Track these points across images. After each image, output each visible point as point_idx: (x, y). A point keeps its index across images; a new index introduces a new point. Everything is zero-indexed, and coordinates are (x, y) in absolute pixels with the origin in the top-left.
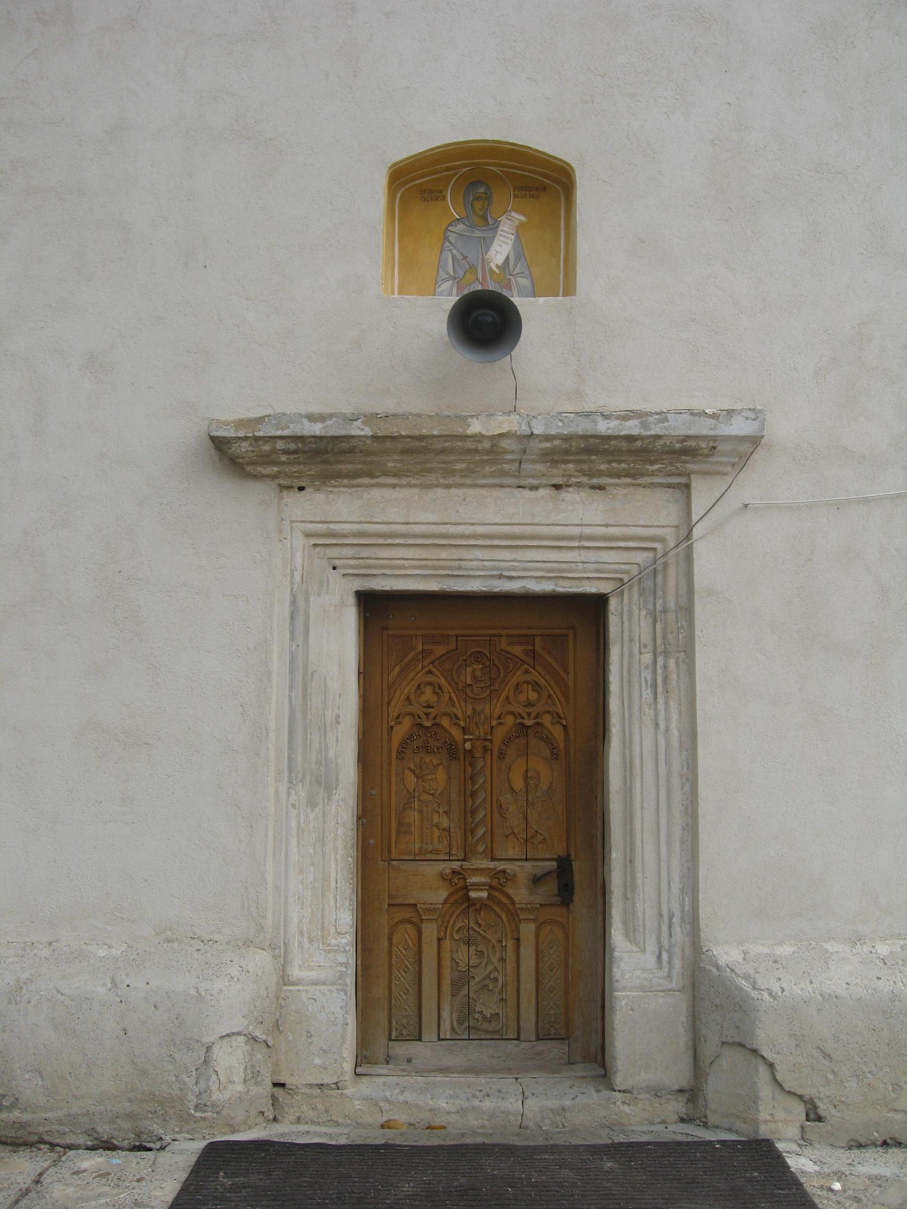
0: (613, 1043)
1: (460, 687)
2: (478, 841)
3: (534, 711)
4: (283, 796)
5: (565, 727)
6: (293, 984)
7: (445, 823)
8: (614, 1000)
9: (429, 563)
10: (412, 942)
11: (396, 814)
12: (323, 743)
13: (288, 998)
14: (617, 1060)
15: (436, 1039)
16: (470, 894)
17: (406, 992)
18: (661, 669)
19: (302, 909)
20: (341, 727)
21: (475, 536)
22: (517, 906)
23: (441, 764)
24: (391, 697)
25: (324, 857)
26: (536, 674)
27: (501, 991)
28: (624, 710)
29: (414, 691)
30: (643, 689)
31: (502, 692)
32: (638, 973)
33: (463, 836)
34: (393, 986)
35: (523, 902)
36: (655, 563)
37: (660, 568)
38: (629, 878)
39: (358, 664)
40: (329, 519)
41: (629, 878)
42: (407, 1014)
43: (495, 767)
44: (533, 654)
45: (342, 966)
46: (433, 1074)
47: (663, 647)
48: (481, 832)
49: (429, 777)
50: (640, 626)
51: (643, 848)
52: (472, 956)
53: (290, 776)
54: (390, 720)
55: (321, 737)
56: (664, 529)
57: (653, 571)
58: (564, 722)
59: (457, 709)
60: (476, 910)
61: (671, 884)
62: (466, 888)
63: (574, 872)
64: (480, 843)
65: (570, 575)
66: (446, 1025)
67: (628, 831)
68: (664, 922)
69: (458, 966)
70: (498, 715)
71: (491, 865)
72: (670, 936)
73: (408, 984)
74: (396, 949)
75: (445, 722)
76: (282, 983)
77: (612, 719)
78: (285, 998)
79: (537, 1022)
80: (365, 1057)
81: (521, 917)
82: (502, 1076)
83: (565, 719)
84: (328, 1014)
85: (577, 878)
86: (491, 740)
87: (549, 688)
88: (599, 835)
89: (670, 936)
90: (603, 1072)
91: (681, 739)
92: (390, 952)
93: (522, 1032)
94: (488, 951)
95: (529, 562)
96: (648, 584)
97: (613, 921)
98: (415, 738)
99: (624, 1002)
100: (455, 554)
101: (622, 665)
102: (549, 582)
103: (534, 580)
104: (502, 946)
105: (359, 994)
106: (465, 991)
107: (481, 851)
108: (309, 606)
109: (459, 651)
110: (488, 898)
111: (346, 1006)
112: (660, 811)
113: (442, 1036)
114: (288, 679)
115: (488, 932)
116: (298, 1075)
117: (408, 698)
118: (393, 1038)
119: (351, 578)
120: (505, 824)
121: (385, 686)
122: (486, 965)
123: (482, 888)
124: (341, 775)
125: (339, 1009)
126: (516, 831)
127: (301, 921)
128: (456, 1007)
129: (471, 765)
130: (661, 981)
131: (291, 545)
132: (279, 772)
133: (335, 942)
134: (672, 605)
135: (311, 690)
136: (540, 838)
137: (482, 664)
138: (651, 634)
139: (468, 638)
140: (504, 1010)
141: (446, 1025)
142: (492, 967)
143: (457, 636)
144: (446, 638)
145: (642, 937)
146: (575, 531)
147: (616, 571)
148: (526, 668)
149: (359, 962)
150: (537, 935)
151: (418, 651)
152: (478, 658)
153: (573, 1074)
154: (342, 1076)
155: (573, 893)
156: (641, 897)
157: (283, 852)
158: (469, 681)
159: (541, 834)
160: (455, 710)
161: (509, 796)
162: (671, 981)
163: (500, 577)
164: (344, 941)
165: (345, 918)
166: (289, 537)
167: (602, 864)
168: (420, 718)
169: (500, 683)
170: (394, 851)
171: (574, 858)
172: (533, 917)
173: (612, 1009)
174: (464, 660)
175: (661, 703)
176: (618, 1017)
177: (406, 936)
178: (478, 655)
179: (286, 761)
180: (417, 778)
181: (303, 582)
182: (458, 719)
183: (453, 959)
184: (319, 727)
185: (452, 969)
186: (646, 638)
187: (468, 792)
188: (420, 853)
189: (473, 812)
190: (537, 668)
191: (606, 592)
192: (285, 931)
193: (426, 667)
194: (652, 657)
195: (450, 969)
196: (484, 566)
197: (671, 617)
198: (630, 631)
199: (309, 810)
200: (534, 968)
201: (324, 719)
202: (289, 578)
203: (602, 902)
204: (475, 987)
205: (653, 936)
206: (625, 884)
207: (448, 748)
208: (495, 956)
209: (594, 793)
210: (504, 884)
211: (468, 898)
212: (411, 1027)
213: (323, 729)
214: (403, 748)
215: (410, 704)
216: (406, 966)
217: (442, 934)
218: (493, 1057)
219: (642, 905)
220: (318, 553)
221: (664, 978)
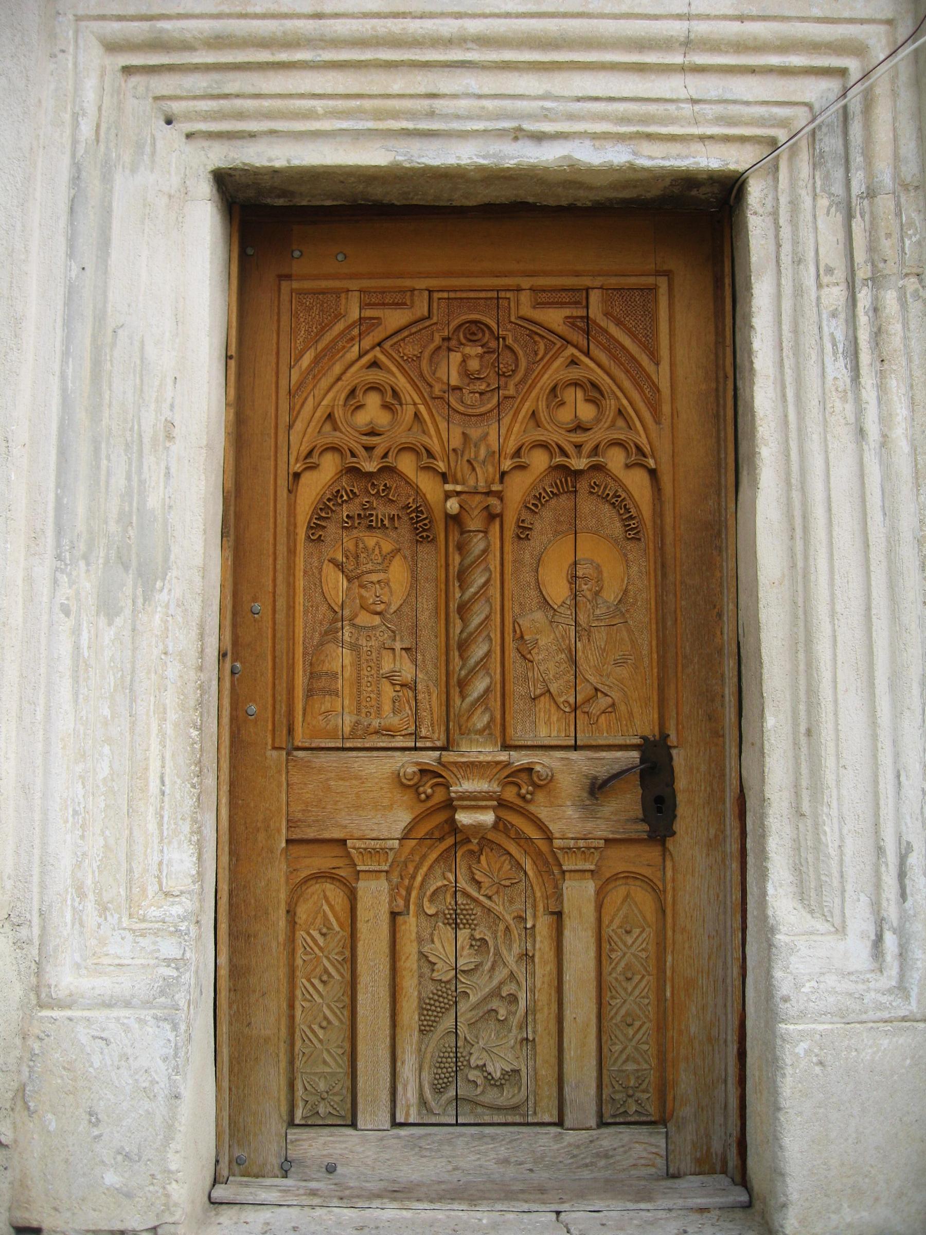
0: (776, 1139)
1: (437, 391)
2: (474, 704)
3: (589, 440)
4: (43, 588)
5: (653, 473)
6: (61, 1005)
7: (407, 671)
8: (779, 1042)
9: (367, 104)
10: (337, 920)
11: (305, 654)
12: (135, 478)
13: (48, 1036)
14: (788, 1180)
15: (387, 1125)
16: (457, 817)
17: (324, 1024)
18: (866, 313)
19: (82, 837)
20: (175, 448)
21: (461, 41)
22: (557, 843)
23: (399, 550)
24: (295, 413)
25: (133, 724)
26: (592, 365)
27: (524, 1025)
28: (785, 407)
29: (341, 402)
30: (829, 359)
31: (523, 401)
32: (831, 981)
33: (444, 697)
34: (298, 1012)
35: (571, 835)
36: (844, 95)
37: (855, 106)
38: (804, 770)
39: (224, 335)
40: (155, 10)
41: (804, 770)
42: (329, 1070)
43: (509, 558)
44: (586, 326)
45: (169, 966)
46: (376, 1203)
47: (869, 267)
48: (479, 686)
49: (374, 577)
50: (816, 229)
51: (836, 701)
52: (463, 948)
53: (58, 545)
54: (292, 461)
55: (130, 464)
56: (865, 27)
57: (841, 111)
58: (651, 463)
59: (430, 437)
60: (471, 852)
61: (903, 778)
62: (449, 806)
63: (676, 769)
64: (479, 711)
65: (664, 130)
66: (409, 1094)
67: (802, 667)
68: (887, 865)
69: (433, 970)
70: (516, 447)
71: (503, 757)
72: (903, 895)
73: (329, 1007)
74: (305, 936)
75: (407, 464)
76: (35, 1002)
77: (760, 429)
78: (42, 1036)
79: (600, 1087)
80: (239, 1162)
81: (565, 868)
82: (526, 1207)
83: (653, 457)
84: (136, 1073)
85: (681, 783)
86: (499, 495)
87: (620, 394)
88: (729, 691)
89: (903, 895)
90: (744, 1198)
91: (916, 460)
92: (291, 939)
93: (568, 1111)
94: (496, 938)
95: (579, 99)
96: (831, 143)
97: (770, 866)
98: (345, 498)
99: (801, 1049)
100: (422, 82)
101: (779, 314)
102: (620, 147)
103: (588, 143)
104: (526, 928)
105: (224, 1028)
106: (448, 1023)
107: (480, 726)
108: (111, 191)
109: (435, 320)
110: (495, 826)
111: (176, 1055)
112: (874, 619)
113: (400, 1118)
114: (59, 338)
115: (495, 898)
116: (68, 1210)
117: (330, 417)
118: (297, 1121)
119: (206, 144)
120: (530, 674)
121: (283, 392)
122: (493, 968)
123: (484, 803)
124: (175, 550)
125: (160, 1062)
126: (554, 688)
127: (79, 865)
128: (428, 1056)
129: (460, 548)
130: (884, 999)
131: (75, 64)
132: (35, 537)
133: (157, 914)
134: (885, 176)
135: (112, 366)
136: (603, 702)
137: (482, 346)
138: (841, 246)
139: (452, 295)
140: (530, 1063)
141: (409, 1094)
142: (505, 972)
143: (430, 292)
144: (409, 294)
145: (837, 901)
146: (677, 28)
147: (761, 122)
148: (573, 354)
149: (223, 960)
150: (599, 907)
151: (350, 321)
152: (474, 334)
153: (680, 1202)
154: (167, 1213)
155: (675, 816)
156: (834, 812)
157: (40, 710)
158: (454, 381)
159: (606, 695)
160: (425, 440)
161: (539, 616)
162: (907, 997)
163: (517, 134)
164: (177, 910)
165: (182, 861)
166: (71, 49)
167: (737, 751)
168: (353, 455)
169: (519, 383)
170: (300, 729)
171: (675, 744)
172: (592, 867)
173: (773, 1063)
174: (443, 339)
175: (869, 387)
176: (789, 1080)
177: (326, 907)
178: (474, 328)
179: (51, 513)
180: (349, 580)
181: (98, 141)
182: (434, 458)
183: (422, 955)
184: (127, 445)
185: (421, 976)
186: (832, 254)
187: (453, 606)
188: (353, 735)
189: (463, 646)
190: (595, 351)
191: (741, 168)
192: (43, 886)
193: (367, 352)
194: (845, 293)
195: (416, 975)
196: (483, 108)
197: (885, 203)
198: (795, 242)
199: (102, 621)
200: (593, 974)
201: (140, 426)
202: (68, 132)
203: (737, 832)
204: (469, 1015)
205: (863, 897)
206: (797, 786)
207: (412, 519)
208: (510, 950)
209: (715, 606)
210: (529, 796)
211: (453, 827)
212: (337, 1099)
213: (135, 448)
214: (320, 518)
215: (336, 428)
216: (326, 971)
217: (401, 902)
218: (506, 1161)
219: (836, 826)
220: (135, 88)
221: (890, 991)
